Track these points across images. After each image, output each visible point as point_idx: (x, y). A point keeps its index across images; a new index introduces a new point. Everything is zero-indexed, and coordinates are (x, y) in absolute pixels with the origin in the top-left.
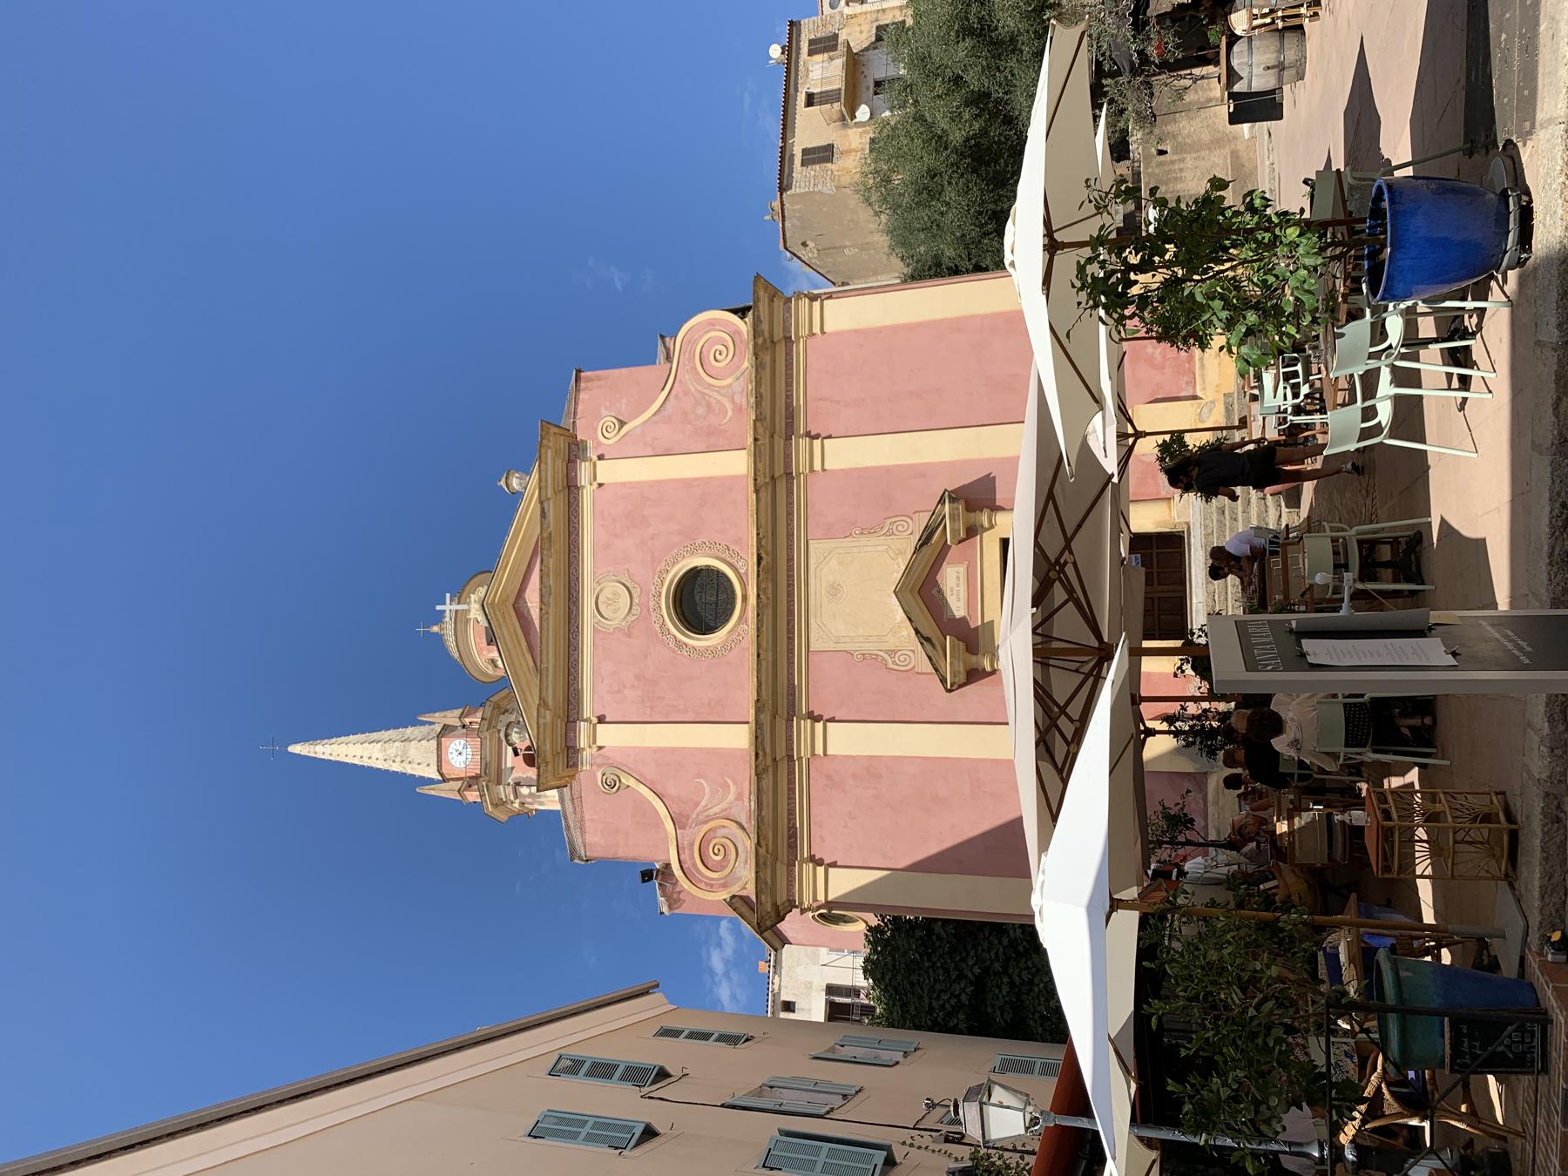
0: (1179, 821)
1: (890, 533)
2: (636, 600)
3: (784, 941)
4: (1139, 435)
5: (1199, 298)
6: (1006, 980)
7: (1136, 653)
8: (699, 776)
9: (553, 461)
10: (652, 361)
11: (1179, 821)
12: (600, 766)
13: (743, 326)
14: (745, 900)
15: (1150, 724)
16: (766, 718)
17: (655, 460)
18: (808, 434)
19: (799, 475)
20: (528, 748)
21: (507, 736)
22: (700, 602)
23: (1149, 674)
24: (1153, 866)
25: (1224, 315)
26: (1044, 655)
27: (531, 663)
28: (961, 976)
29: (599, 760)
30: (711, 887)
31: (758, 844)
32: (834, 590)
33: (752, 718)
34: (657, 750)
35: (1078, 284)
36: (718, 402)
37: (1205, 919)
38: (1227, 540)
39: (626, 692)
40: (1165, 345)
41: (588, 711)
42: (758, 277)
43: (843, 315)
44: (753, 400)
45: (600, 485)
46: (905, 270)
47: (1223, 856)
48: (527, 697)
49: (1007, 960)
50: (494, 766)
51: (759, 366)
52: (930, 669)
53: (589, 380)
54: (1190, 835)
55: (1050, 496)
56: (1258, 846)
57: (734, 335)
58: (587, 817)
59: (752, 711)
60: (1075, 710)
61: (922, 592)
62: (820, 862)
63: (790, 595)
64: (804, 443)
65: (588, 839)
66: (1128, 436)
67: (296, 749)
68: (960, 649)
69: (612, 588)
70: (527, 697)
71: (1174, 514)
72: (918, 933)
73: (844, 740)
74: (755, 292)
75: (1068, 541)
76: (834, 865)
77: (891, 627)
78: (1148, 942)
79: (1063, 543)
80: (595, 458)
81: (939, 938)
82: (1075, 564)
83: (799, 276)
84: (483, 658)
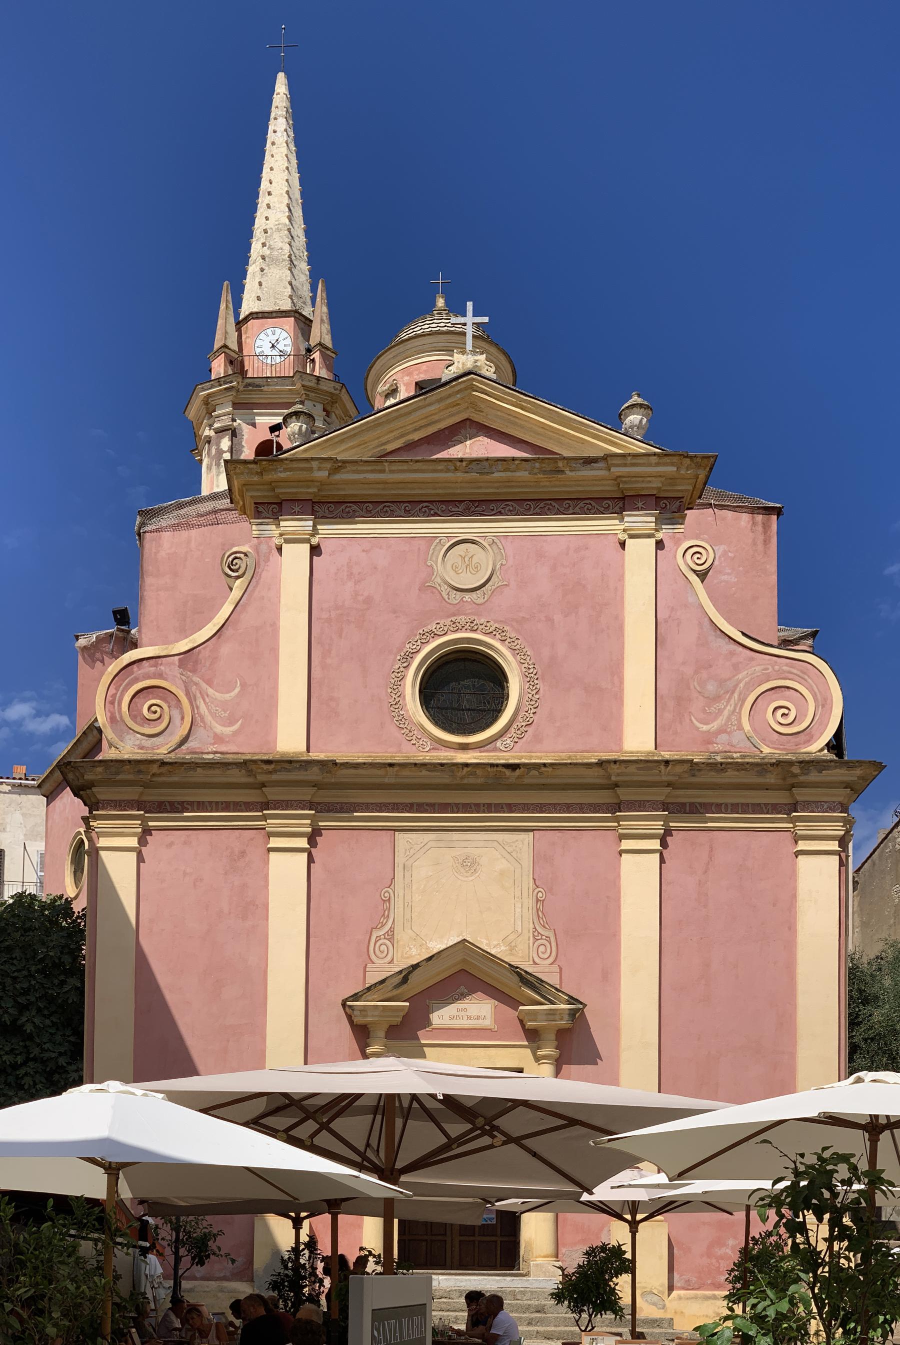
0: (201, 1250)
1: (536, 935)
2: (467, 597)
3: (50, 797)
4: (634, 1226)
5: (793, 1288)
6: (19, 1059)
7: (386, 1209)
8: (243, 685)
9: (659, 474)
10: (785, 617)
11: (201, 1250)
12: (257, 549)
13: (817, 746)
14: (97, 746)
15: (306, 1223)
16: (313, 774)
17: (653, 622)
18: (668, 832)
19: (617, 820)
20: (279, 447)
21: (297, 414)
22: (463, 685)
23: (360, 1226)
24: (151, 1220)
25: (771, 1313)
26: (388, 1107)
27: (390, 447)
28: (23, 1008)
29: (264, 548)
30: (111, 702)
31: (163, 763)
32: (469, 865)
33: (314, 755)
34: (275, 628)
35: (826, 1155)
36: (721, 711)
37: (99, 1268)
38: (509, 1312)
39: (350, 584)
40: (736, 1257)
41: (330, 532)
42: (880, 767)
43: (817, 881)
44: (719, 759)
45: (623, 544)
46: (865, 960)
47: (164, 1294)
48: (347, 443)
49: (43, 1062)
50: (255, 397)
51: (763, 767)
52: (370, 981)
53: (766, 527)
54: (186, 1261)
55: (572, 1122)
56: (176, 1329)
57: (807, 734)
58: (194, 532)
59: (322, 756)
60: (324, 1139)
61: (463, 973)
62: (143, 842)
63: (466, 808)
64: (658, 826)
65: (166, 535)
66: (634, 1214)
67: (281, 78)
68: (397, 1014)
69: (484, 561)
70: (347, 443)
71: (540, 1261)
72: (67, 959)
73: (286, 872)
74: (860, 763)
75: (517, 1141)
76: (140, 859)
77: (421, 935)
78: (74, 1204)
79: (515, 1134)
80: (659, 536)
81: (63, 983)
82: (491, 1147)
83: (875, 822)
84: (400, 376)
